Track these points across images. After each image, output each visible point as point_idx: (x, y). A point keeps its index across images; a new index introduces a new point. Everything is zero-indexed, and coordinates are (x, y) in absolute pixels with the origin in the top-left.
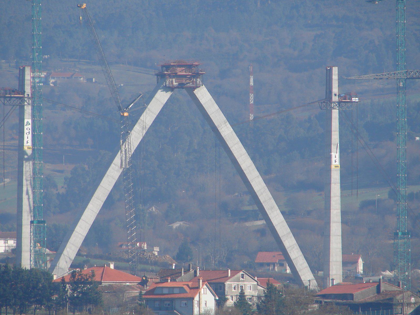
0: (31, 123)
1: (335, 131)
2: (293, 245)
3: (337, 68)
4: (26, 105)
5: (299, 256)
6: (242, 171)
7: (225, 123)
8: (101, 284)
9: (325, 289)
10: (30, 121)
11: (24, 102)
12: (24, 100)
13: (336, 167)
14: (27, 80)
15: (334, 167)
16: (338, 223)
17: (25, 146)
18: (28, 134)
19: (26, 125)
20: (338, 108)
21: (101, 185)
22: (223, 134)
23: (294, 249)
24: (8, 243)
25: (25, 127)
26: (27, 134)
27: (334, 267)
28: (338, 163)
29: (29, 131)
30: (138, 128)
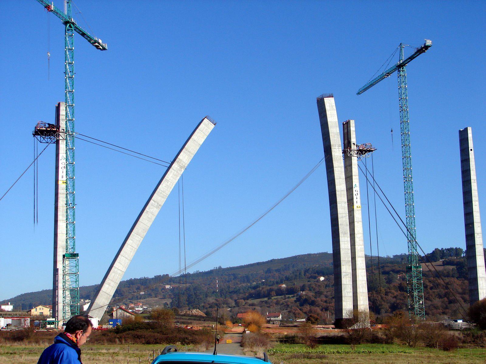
2: (349, 273)
3: (212, 126)
4: (61, 139)
8: (44, 326)
9: (387, 313)
11: (59, 137)
12: (59, 135)
14: (63, 115)
18: (357, 195)
20: (356, 155)
21: (363, 258)
23: (347, 276)
26: (357, 195)
29: (357, 192)
30: (176, 166)
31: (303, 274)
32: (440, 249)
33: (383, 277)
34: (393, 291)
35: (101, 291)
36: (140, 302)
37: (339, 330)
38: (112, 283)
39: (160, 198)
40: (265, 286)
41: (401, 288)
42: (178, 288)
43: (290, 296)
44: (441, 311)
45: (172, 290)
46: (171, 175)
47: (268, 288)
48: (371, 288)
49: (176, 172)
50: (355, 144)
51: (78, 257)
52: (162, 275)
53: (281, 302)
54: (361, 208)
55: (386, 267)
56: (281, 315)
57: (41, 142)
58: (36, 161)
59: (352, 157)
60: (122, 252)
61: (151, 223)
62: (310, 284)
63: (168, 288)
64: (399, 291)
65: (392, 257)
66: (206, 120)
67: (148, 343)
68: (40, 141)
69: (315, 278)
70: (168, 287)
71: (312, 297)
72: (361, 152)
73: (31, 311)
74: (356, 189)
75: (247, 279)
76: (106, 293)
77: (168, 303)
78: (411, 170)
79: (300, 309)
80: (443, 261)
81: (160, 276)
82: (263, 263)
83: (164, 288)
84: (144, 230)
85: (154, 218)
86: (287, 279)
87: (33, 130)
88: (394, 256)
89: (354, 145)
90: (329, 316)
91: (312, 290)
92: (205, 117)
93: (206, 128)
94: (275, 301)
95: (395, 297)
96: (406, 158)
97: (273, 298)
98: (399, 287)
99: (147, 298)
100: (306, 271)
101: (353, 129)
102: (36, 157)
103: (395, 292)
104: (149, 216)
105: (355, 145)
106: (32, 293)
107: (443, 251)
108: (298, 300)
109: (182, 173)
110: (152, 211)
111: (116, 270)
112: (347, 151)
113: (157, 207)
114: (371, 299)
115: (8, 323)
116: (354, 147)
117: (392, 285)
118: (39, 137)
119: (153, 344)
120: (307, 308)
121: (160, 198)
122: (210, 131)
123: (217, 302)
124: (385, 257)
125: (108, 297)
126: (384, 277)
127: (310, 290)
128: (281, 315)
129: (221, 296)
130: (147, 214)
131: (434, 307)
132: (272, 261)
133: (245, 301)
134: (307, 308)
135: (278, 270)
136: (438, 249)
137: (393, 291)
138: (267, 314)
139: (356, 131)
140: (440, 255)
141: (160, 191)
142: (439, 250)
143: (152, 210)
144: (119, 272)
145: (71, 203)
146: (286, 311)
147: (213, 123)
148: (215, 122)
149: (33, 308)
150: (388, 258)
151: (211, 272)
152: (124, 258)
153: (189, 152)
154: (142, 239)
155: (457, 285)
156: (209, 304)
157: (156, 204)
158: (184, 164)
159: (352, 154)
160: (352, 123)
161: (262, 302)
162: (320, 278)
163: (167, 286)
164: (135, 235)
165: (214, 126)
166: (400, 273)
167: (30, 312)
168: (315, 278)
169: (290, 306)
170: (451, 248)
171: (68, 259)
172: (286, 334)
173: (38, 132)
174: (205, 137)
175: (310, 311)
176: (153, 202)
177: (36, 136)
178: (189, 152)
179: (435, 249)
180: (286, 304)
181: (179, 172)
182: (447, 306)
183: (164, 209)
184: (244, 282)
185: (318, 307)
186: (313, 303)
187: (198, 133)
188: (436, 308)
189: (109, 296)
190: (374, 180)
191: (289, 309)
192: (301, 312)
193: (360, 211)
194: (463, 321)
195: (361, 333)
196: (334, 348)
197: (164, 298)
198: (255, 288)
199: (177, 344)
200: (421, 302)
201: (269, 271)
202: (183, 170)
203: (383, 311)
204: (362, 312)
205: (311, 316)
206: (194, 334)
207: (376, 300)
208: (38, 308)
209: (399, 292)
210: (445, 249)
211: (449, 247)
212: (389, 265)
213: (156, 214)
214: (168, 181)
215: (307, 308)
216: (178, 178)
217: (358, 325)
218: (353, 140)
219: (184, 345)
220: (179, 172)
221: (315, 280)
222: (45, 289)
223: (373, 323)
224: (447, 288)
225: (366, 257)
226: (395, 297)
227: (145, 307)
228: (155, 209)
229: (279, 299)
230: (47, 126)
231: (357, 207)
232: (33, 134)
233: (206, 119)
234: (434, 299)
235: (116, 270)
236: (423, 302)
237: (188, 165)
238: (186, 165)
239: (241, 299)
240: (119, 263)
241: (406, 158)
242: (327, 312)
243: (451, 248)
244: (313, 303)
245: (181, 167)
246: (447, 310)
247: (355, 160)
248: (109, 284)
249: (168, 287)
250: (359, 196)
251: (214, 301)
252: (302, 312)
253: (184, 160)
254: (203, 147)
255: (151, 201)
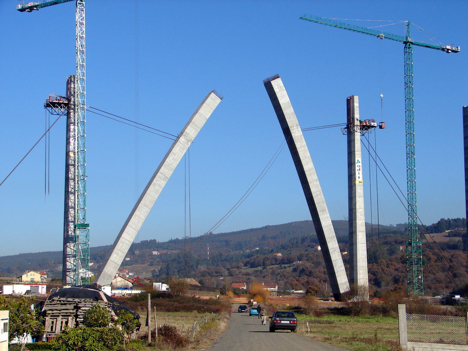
0: (360, 161)
1: (358, 151)
3: (219, 101)
5: (339, 259)
6: (304, 172)
7: (297, 126)
10: (360, 160)
13: (359, 182)
15: (358, 183)
16: (363, 232)
17: (412, 210)
18: (359, 170)
19: (357, 163)
22: (293, 135)
23: (335, 252)
24: (408, 342)
25: (356, 165)
27: (361, 271)
28: (361, 179)
30: (183, 140)
31: (300, 242)
32: (446, 219)
33: (386, 248)
34: (394, 263)
35: (109, 261)
36: (125, 269)
37: (339, 303)
38: (120, 253)
39: (167, 171)
40: (259, 255)
41: (404, 261)
42: (166, 254)
43: (287, 265)
44: (444, 285)
45: (160, 256)
46: (178, 148)
47: (264, 256)
48: (371, 258)
49: (182, 146)
50: (359, 120)
51: (89, 227)
52: (149, 241)
53: (277, 272)
54: (363, 183)
55: (388, 238)
56: (277, 286)
57: (52, 114)
58: (47, 134)
59: (356, 133)
60: (130, 223)
61: (158, 195)
62: (308, 254)
63: (155, 255)
64: (401, 264)
65: (395, 226)
66: (213, 95)
67: (168, 310)
68: (51, 112)
69: (313, 247)
70: (155, 253)
71: (309, 267)
72: (365, 127)
73: (21, 277)
74: (358, 157)
75: (239, 246)
76: (114, 262)
77: (157, 270)
78: (414, 146)
79: (297, 280)
80: (449, 233)
81: (147, 241)
82: (257, 230)
83: (151, 255)
84: (151, 202)
85: (161, 190)
86: (283, 248)
87: (45, 102)
88: (397, 225)
89: (358, 120)
90: (327, 288)
91: (310, 260)
92: (212, 90)
93: (213, 102)
94: (271, 271)
95: (397, 270)
96: (410, 134)
97: (268, 267)
98: (401, 258)
99: (133, 265)
100: (303, 240)
101: (356, 105)
102: (48, 128)
103: (397, 265)
104: (157, 188)
105: (359, 121)
106: (8, 257)
107: (450, 221)
108: (295, 270)
109: (189, 146)
110: (159, 183)
111: (124, 240)
112: (351, 126)
113: (164, 180)
114: (371, 272)
115: (27, 290)
116: (357, 123)
117: (393, 257)
118: (50, 109)
119: (172, 311)
120: (304, 279)
121: (167, 171)
122: (217, 105)
123: (209, 271)
124: (388, 226)
125: (116, 266)
126: (386, 248)
127: (308, 260)
128: (277, 286)
129: (213, 264)
130: (155, 186)
131: (437, 281)
132: (267, 228)
133: (238, 270)
134: (304, 279)
135: (274, 238)
136: (444, 219)
137: (394, 263)
138: (263, 285)
139: (360, 107)
140: (446, 226)
141: (168, 164)
142: (445, 221)
143: (159, 182)
144: (127, 242)
145: (82, 175)
146: (283, 281)
147: (219, 97)
148: (221, 97)
149: (23, 274)
150: (391, 227)
151: (201, 238)
152: (132, 229)
153: (196, 126)
154: (149, 210)
155: (462, 258)
156: (200, 272)
157: (163, 177)
158: (191, 138)
159: (355, 129)
160: (356, 99)
161: (257, 271)
162: (318, 247)
163: (154, 252)
164: (143, 206)
165: (221, 100)
166: (404, 244)
167: (21, 278)
168: (313, 247)
169: (287, 276)
170: (458, 218)
171: (78, 229)
172: (288, 305)
173: (50, 105)
174: (212, 111)
175: (308, 282)
176: (161, 175)
177: (47, 108)
178: (196, 126)
179: (441, 219)
180: (281, 274)
181: (186, 145)
182: (450, 280)
183: (171, 182)
184: (236, 250)
185: (316, 278)
186: (310, 274)
187: (205, 107)
188: (439, 281)
189: (117, 265)
190: (376, 154)
191: (285, 280)
192: (298, 283)
193: (362, 187)
194: (461, 297)
195: (360, 306)
196: (337, 318)
197: (151, 265)
198: (249, 256)
199: (194, 312)
200: (420, 277)
201: (264, 238)
202: (190, 144)
203: (383, 284)
204: (361, 287)
205: (310, 288)
206: (207, 303)
207: (377, 272)
208: (29, 274)
209: (401, 264)
210: (452, 220)
211: (456, 218)
212: (392, 235)
213: (163, 186)
214: (175, 154)
215: (304, 279)
216: (185, 151)
217: (357, 299)
218: (357, 116)
219: (200, 313)
220: (186, 145)
221: (313, 249)
222: (22, 253)
223: (371, 297)
224: (451, 261)
225: (367, 225)
226: (397, 270)
227: (131, 274)
228: (162, 181)
229: (274, 269)
230: (59, 98)
231: (359, 182)
232: (45, 106)
233: (212, 93)
234: (437, 272)
235: (124, 240)
236: (421, 277)
237: (195, 139)
238: (193, 139)
239: (235, 268)
240: (127, 233)
241: (410, 134)
242: (325, 284)
243: (458, 218)
244: (310, 274)
245: (188, 141)
246: (450, 284)
247: (358, 136)
248: (117, 254)
249: (155, 253)
250: (361, 172)
251: (205, 269)
252: (299, 282)
253: (191, 134)
254: (210, 121)
255: (159, 174)
